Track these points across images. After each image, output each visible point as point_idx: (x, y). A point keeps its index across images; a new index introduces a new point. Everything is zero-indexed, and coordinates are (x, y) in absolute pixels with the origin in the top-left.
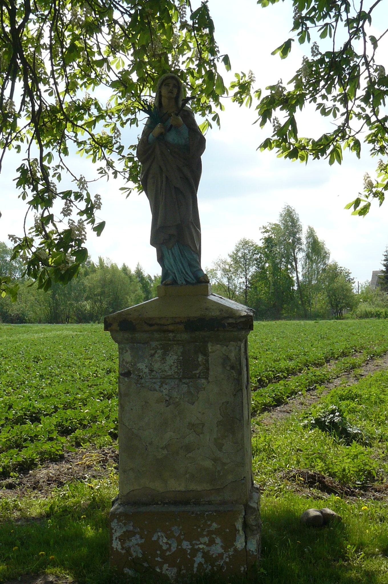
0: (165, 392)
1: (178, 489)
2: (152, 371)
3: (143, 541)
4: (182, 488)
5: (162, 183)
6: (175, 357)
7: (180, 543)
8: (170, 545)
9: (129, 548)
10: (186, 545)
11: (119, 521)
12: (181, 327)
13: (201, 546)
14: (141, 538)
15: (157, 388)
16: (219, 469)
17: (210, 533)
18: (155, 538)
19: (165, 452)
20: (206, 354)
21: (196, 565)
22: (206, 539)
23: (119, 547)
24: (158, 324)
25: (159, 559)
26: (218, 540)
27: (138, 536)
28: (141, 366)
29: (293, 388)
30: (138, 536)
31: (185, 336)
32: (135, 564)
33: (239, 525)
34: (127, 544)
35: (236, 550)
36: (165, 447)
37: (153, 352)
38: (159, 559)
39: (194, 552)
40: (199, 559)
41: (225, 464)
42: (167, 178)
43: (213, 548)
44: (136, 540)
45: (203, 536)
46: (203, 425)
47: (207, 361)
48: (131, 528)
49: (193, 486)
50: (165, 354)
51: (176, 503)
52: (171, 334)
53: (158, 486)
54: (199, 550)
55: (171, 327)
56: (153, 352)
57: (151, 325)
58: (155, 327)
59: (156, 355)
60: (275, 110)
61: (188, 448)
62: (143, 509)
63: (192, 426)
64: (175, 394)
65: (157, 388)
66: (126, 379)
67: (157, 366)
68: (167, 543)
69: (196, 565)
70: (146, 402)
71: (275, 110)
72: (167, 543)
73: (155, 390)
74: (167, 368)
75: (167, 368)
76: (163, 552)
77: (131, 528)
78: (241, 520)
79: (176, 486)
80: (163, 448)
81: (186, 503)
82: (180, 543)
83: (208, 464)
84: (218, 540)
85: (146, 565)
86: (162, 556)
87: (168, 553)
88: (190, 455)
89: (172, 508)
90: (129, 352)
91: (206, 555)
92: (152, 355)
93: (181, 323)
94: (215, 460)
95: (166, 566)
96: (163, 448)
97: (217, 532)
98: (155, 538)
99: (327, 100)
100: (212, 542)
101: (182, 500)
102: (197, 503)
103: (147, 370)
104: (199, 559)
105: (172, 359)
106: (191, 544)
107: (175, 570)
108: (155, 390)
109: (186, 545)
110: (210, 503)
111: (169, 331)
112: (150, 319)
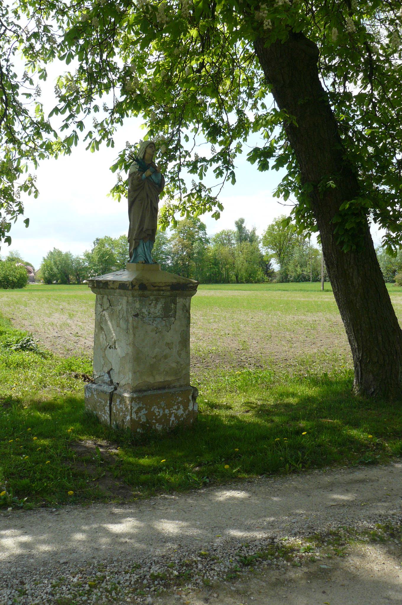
0: (155, 325)
1: (160, 381)
2: (149, 313)
3: (147, 412)
4: (162, 380)
5: (148, 204)
6: (161, 305)
7: (164, 411)
8: (159, 412)
9: (140, 417)
10: (167, 411)
11: (136, 402)
12: (169, 288)
13: (174, 411)
14: (146, 410)
15: (151, 323)
16: (179, 367)
17: (178, 403)
18: (152, 410)
19: (155, 360)
20: (175, 304)
21: (171, 422)
22: (176, 407)
23: (135, 417)
24: (158, 286)
25: (154, 421)
26: (181, 407)
27: (144, 409)
28: (144, 310)
29: (286, 299)
30: (144, 409)
31: (168, 293)
32: (143, 426)
33: (190, 398)
34: (140, 414)
35: (189, 411)
36: (155, 357)
37: (151, 302)
38: (154, 421)
39: (171, 414)
40: (172, 418)
41: (181, 365)
42: (151, 201)
43: (179, 411)
44: (144, 412)
45: (174, 405)
46: (173, 343)
47: (176, 307)
48: (141, 405)
49: (168, 379)
50: (156, 304)
51: (159, 389)
52: (162, 292)
53: (151, 380)
54: (173, 413)
55: (164, 288)
56: (151, 302)
57: (155, 287)
58: (156, 288)
59: (152, 304)
60: (108, 93)
61: (166, 357)
62: (145, 393)
63: (168, 344)
64: (159, 327)
65: (151, 323)
66: (136, 318)
67: (152, 310)
68: (158, 412)
69: (171, 422)
70: (146, 332)
71: (108, 93)
72: (158, 412)
73: (150, 324)
74: (157, 312)
75: (157, 312)
76: (156, 416)
77: (141, 405)
78: (191, 395)
79: (160, 379)
80: (153, 358)
81: (164, 388)
82: (164, 411)
83: (174, 365)
84: (181, 407)
85: (148, 425)
86: (156, 420)
87: (159, 417)
88: (166, 361)
89: (156, 392)
90: (138, 302)
91: (176, 416)
92: (150, 304)
93: (169, 285)
94: (177, 363)
95: (157, 425)
96: (153, 358)
97: (181, 402)
98: (152, 410)
99: (187, 128)
100: (179, 408)
101: (162, 387)
102: (169, 388)
103: (147, 313)
104: (172, 418)
105: (160, 306)
106: (170, 411)
107: (161, 426)
108: (150, 324)
109: (167, 411)
110: (174, 387)
111: (162, 290)
112: (155, 283)
